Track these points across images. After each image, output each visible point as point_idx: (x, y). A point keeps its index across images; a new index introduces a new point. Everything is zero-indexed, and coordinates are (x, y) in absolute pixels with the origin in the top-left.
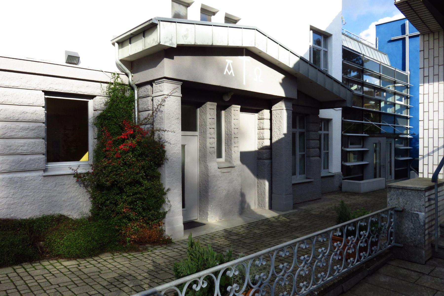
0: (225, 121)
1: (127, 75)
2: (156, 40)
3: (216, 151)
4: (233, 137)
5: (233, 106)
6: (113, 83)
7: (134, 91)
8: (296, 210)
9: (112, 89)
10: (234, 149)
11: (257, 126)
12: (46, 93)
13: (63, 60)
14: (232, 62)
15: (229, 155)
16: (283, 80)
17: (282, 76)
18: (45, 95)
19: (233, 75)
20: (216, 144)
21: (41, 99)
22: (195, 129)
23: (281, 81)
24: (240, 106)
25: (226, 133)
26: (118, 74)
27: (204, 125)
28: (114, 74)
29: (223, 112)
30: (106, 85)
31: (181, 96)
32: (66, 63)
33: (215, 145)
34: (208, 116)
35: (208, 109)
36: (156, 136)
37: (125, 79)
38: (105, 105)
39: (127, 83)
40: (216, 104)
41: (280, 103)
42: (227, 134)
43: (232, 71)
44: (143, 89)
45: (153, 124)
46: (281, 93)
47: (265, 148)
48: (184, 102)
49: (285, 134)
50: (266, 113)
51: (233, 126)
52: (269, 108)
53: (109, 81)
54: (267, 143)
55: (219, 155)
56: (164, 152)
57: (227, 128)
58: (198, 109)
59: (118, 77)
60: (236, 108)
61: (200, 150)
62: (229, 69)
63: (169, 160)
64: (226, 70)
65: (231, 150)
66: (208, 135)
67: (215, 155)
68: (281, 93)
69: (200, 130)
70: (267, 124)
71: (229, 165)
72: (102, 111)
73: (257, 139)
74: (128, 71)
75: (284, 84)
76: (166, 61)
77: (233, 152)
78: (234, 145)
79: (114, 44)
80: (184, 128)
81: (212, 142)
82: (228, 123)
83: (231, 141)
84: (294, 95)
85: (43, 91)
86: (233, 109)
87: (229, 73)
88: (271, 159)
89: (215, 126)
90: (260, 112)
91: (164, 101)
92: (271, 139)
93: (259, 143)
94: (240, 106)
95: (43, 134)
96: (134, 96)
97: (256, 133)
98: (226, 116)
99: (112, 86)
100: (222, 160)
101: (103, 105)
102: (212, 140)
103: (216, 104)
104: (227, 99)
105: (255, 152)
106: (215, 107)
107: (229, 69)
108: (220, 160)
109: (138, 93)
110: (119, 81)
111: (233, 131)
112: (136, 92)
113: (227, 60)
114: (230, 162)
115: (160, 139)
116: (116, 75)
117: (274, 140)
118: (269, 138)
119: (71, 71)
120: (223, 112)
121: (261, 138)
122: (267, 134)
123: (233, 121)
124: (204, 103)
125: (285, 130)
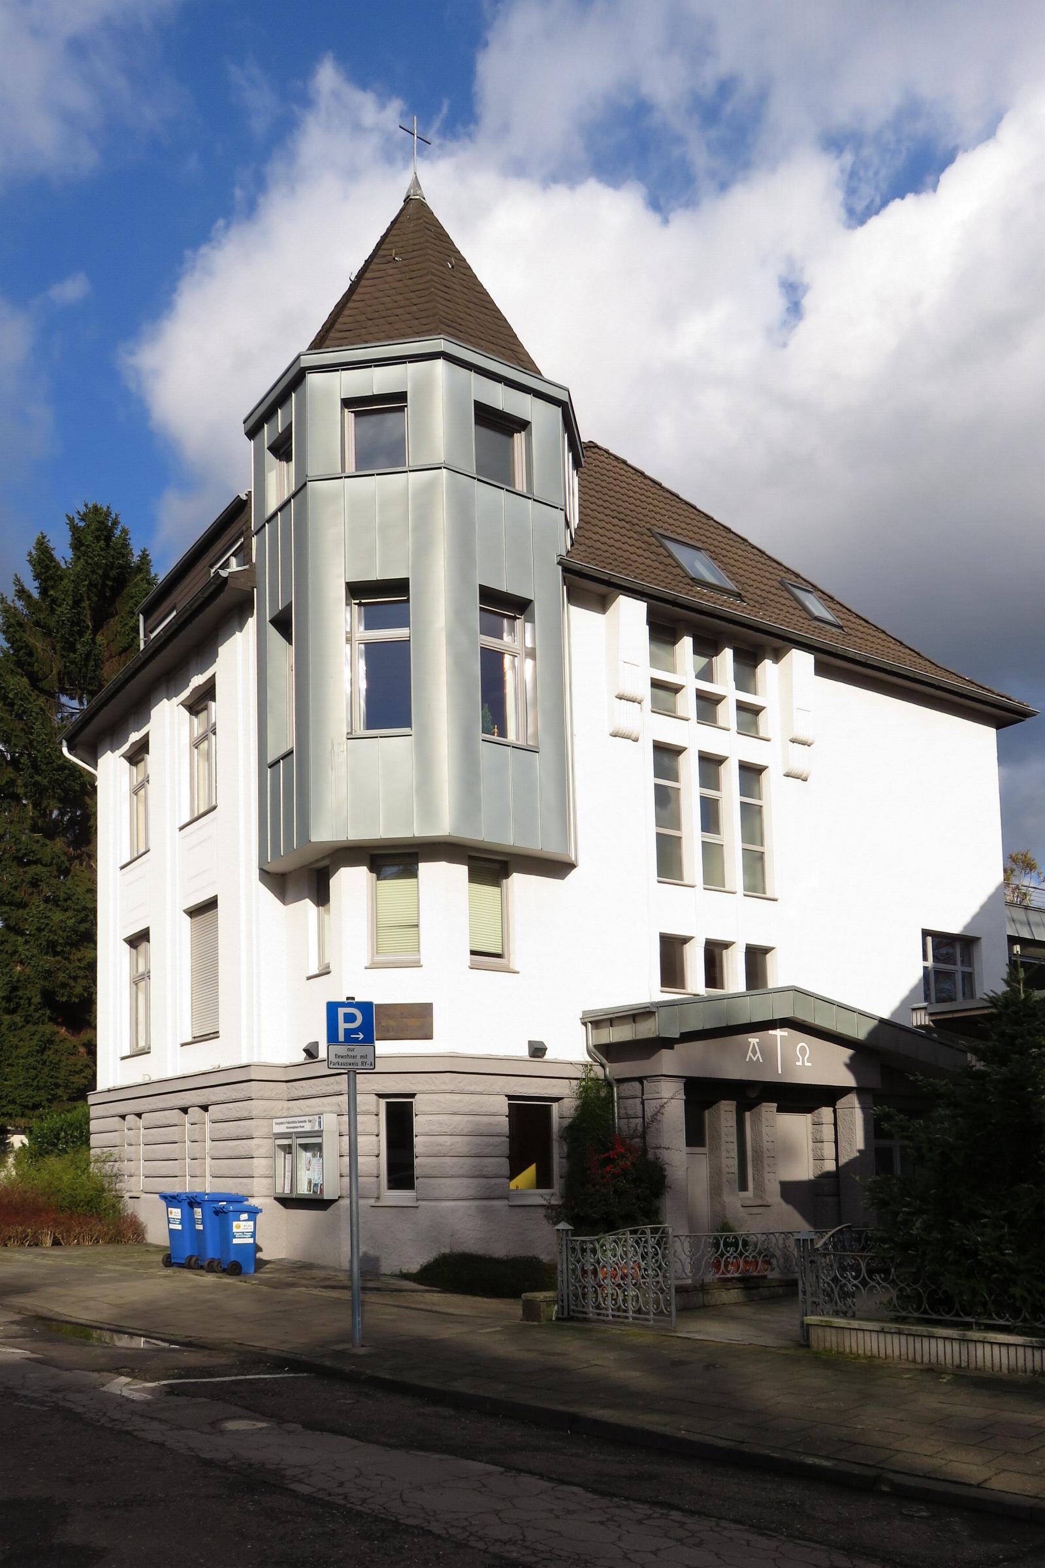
0: (752, 1129)
1: (602, 1065)
2: (653, 1030)
3: (737, 1178)
4: (765, 1155)
5: (764, 1104)
6: (584, 1079)
7: (612, 1090)
8: (246, 567)
9: (584, 1087)
10: (767, 1176)
11: (810, 1136)
12: (510, 1097)
13: (524, 1052)
14: (758, 1040)
15: (760, 1187)
16: (852, 1058)
17: (849, 1052)
18: (509, 1100)
19: (761, 1061)
20: (736, 1167)
21: (503, 1105)
22: (703, 1145)
23: (847, 1061)
24: (776, 1105)
25: (753, 1150)
26: (591, 1065)
27: (717, 1136)
28: (586, 1066)
29: (748, 1114)
30: (574, 1082)
31: (684, 1098)
32: (531, 1057)
33: (735, 1169)
34: (723, 1123)
35: (722, 1113)
36: (650, 1156)
37: (598, 1072)
38: (576, 1110)
39: (602, 1077)
40: (735, 1103)
41: (850, 1095)
42: (755, 1151)
43: (758, 1054)
44: (626, 1086)
45: (644, 1138)
46: (849, 1080)
47: (827, 1175)
48: (687, 1103)
49: (859, 1151)
50: (826, 1113)
51: (765, 1138)
52: (832, 1104)
53: (579, 1077)
54: (830, 1166)
55: (743, 1187)
56: (664, 1177)
57: (754, 1140)
58: (706, 1112)
59: (591, 1070)
60: (771, 1107)
61: (711, 1177)
62: (754, 1052)
63: (545, 1222)
64: (750, 1054)
65: (763, 1177)
66: (724, 1154)
67: (736, 1185)
68: (849, 1080)
69: (709, 1145)
70: (828, 1132)
71: (760, 1202)
72: (570, 1120)
73: (811, 1161)
74: (604, 1061)
75: (852, 1066)
76: (665, 1053)
77: (766, 1182)
78: (767, 1169)
79: (585, 1024)
80: (689, 1143)
81: (730, 1163)
82: (757, 1134)
83: (762, 1162)
84: (875, 1082)
85: (506, 1096)
86: (763, 1109)
87: (755, 1059)
88: (838, 1194)
89: (734, 1139)
90: (816, 1111)
91: (662, 1106)
92: (837, 1160)
93: (815, 1166)
94: (776, 1105)
95: (505, 1150)
96: (612, 1096)
97: (810, 1148)
98: (753, 1122)
99: (584, 1083)
100: (750, 1193)
101: (572, 1111)
102: (730, 1162)
103: (735, 1103)
104: (753, 1095)
105: (810, 1182)
106: (734, 1109)
107: (754, 1052)
108: (743, 1194)
109: (617, 1090)
110: (592, 1075)
111: (766, 1145)
112: (615, 1089)
113: (750, 1040)
114: (761, 1197)
115: (658, 1159)
116: (589, 1067)
117: (843, 1160)
118: (834, 1157)
119: (535, 1067)
120: (748, 1114)
121: (819, 1159)
122: (829, 1150)
123: (765, 1130)
124: (716, 1102)
125: (860, 1144)
